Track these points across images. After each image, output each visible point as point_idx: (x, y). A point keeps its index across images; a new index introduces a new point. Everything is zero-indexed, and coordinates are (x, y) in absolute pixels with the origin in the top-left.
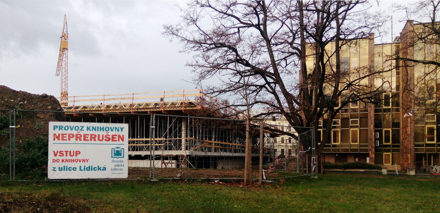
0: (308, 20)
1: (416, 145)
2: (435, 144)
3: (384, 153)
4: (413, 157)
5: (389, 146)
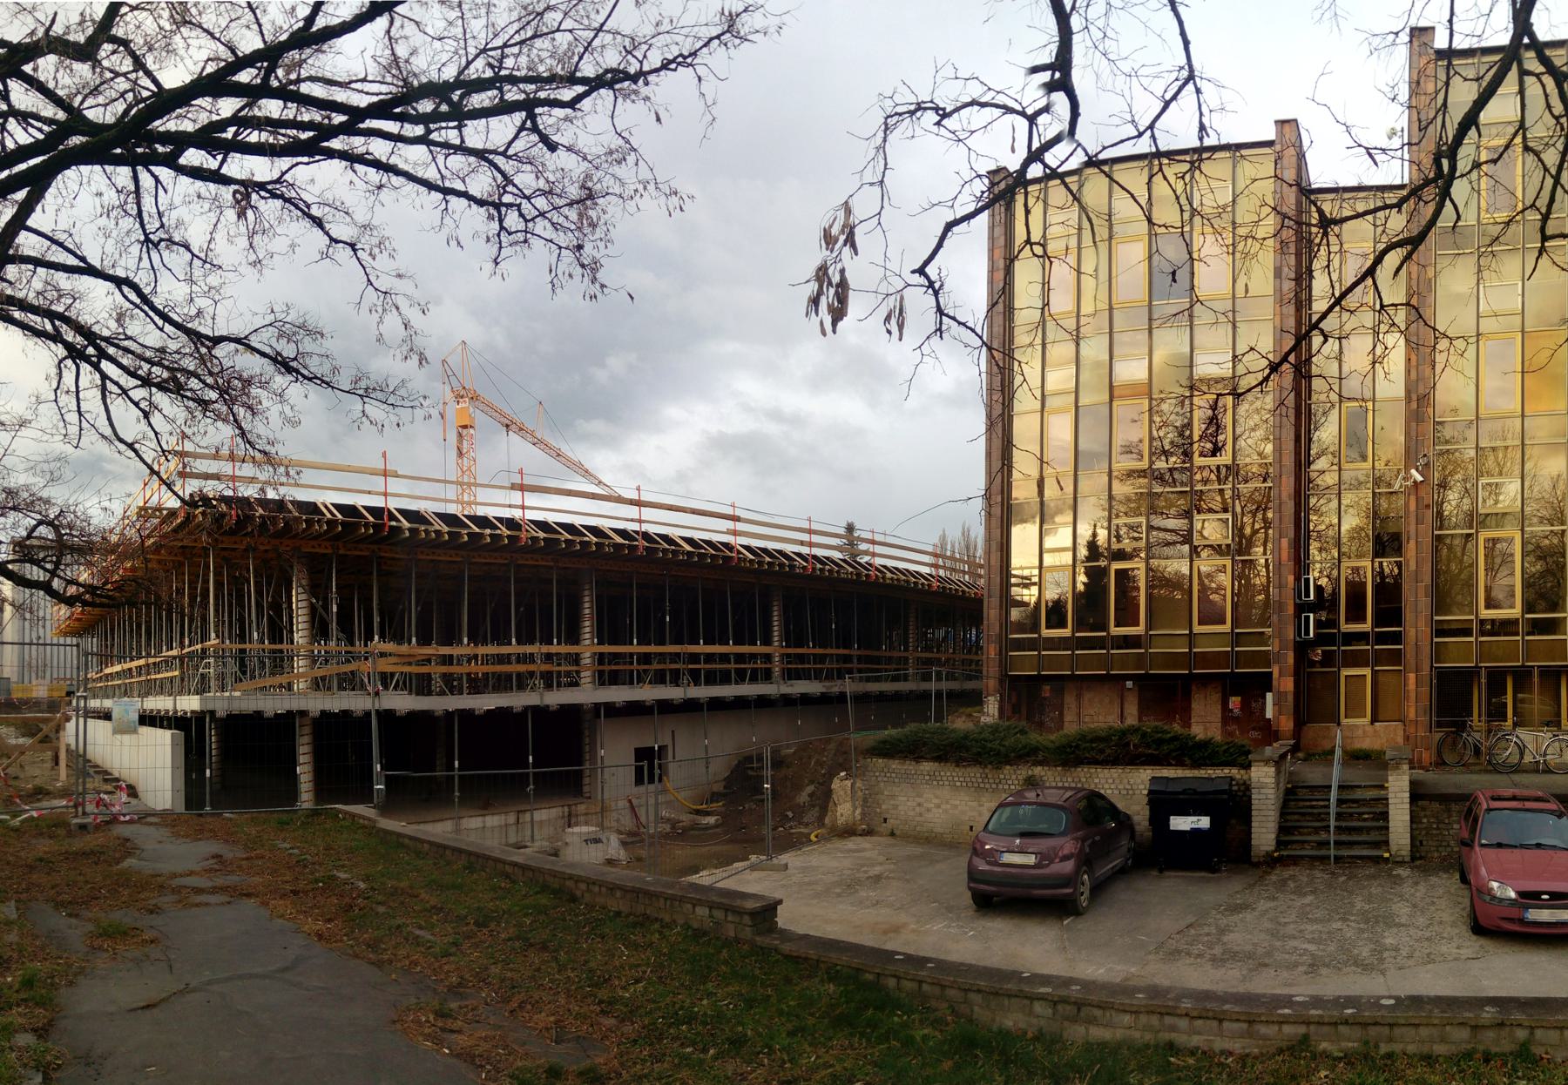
0: (1206, 210)
1: (1441, 632)
2: (1515, 622)
3: (1346, 672)
4: (1425, 689)
5: (1362, 637)
